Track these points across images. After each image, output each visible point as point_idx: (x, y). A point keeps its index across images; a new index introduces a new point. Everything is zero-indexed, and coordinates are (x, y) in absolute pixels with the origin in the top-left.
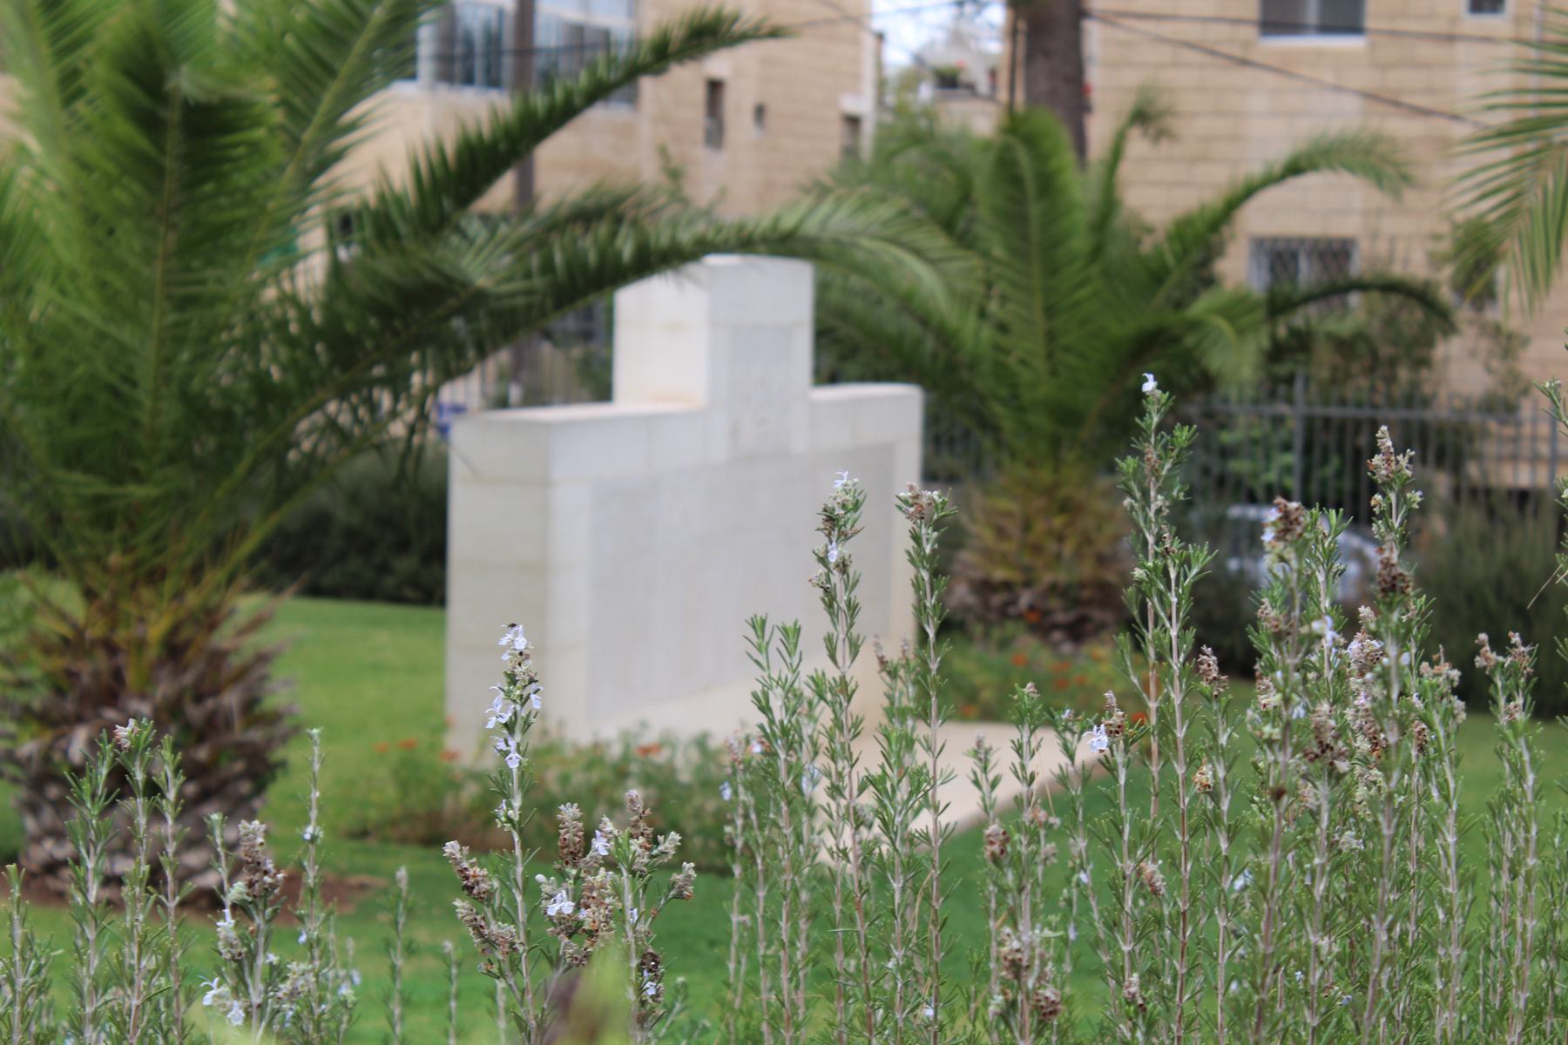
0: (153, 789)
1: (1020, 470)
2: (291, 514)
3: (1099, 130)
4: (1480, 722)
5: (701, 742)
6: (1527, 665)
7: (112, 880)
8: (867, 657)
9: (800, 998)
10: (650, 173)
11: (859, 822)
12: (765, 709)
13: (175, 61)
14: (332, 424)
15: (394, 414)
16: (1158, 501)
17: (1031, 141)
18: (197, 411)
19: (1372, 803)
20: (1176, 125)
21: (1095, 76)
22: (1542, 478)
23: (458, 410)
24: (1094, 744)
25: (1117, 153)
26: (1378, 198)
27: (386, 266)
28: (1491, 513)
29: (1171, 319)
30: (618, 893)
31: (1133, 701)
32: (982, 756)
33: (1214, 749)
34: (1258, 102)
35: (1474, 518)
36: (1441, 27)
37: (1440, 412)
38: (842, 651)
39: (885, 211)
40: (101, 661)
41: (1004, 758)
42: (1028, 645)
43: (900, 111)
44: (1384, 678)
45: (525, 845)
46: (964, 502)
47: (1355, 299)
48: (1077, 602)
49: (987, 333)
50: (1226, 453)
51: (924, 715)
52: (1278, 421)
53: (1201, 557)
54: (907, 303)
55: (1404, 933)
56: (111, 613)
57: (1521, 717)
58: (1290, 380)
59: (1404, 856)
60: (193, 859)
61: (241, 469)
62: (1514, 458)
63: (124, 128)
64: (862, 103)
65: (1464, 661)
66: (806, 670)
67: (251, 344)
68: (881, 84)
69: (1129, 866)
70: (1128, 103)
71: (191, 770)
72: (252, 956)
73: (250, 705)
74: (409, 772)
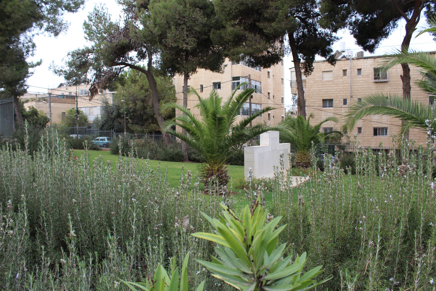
0: (216, 183)
1: (300, 151)
2: (229, 157)
3: (307, 117)
4: (346, 175)
5: (269, 178)
6: (351, 169)
7: (212, 192)
8: (285, 169)
9: (279, 203)
10: (263, 123)
11: (285, 186)
12: (275, 175)
13: (217, 114)
14: (233, 148)
15: (239, 147)
16: (313, 153)
17: (300, 119)
18: (220, 147)
19: (335, 183)
20: (315, 117)
21: (306, 112)
22: (352, 151)
23: (245, 146)
24: (308, 178)
25: (309, 119)
26: (335, 123)
27: (237, 132)
28: (347, 154)
29: (315, 136)
30: (261, 193)
31: (311, 174)
32: (297, 179)
33: (320, 178)
34: (323, 114)
35: (346, 155)
36: (340, 106)
37: (342, 144)
38: (282, 169)
39: (286, 126)
40: (211, 171)
41: (299, 179)
42: (301, 168)
43: (287, 116)
44: (336, 170)
45: (252, 188)
46: (295, 154)
47: (333, 133)
48: (306, 164)
49: (297, 137)
50: (321, 149)
51: (291, 176)
52: (326, 145)
53: (318, 159)
54: (289, 135)
55: (339, 196)
56: (212, 167)
57: (350, 174)
58: (327, 141)
59: (339, 188)
60: (220, 190)
61: (224, 153)
62: (349, 149)
63: (212, 120)
64: (284, 115)
65: (345, 169)
66: (279, 171)
67: (225, 141)
68: (285, 113)
69: (311, 190)
70: (310, 115)
71: (220, 182)
72: (226, 199)
73: (225, 175)
74: (241, 182)
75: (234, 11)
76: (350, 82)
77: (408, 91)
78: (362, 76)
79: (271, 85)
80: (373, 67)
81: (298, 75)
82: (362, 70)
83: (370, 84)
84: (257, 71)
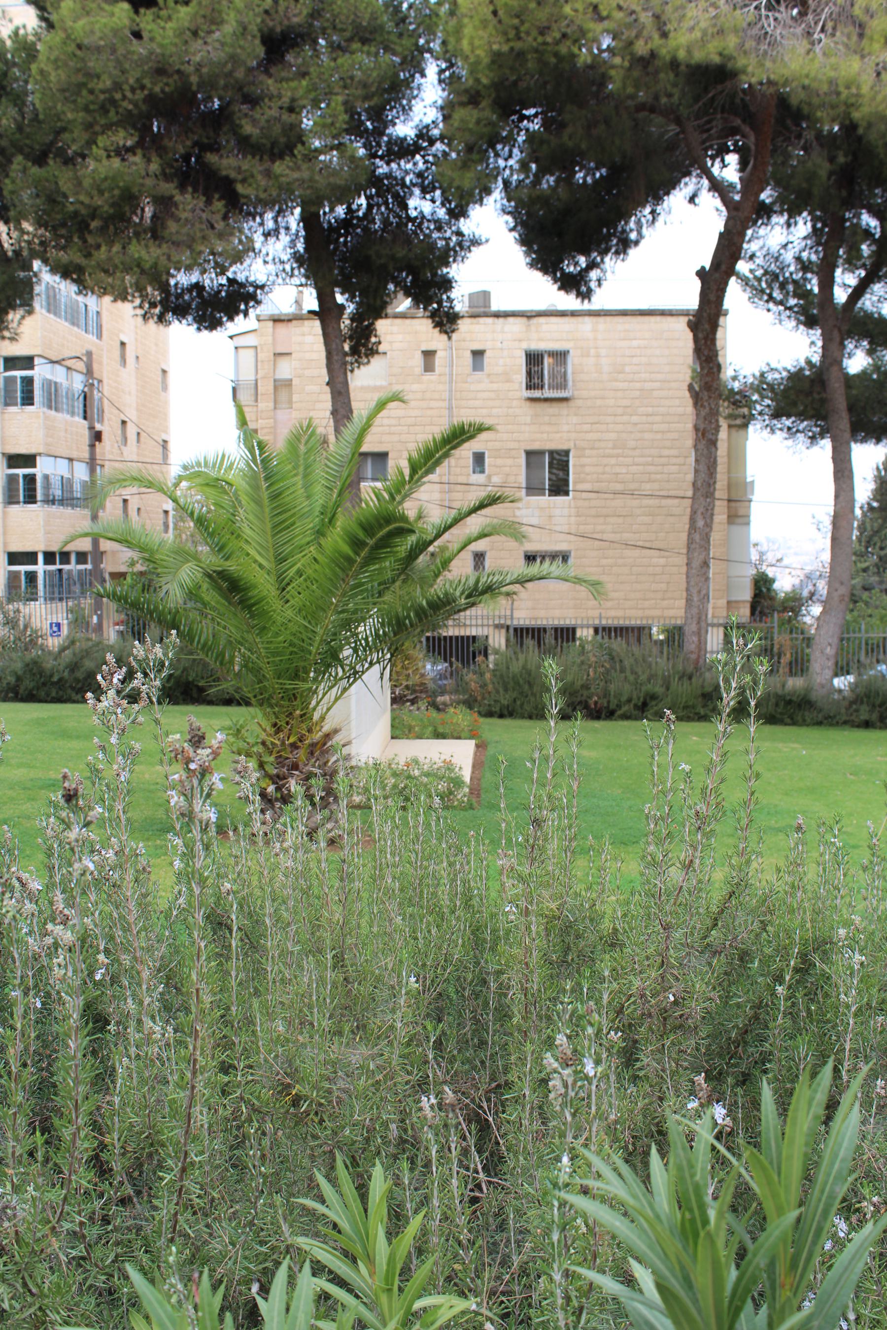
48: (414, 691)
75: (129, 95)
76: (446, 395)
77: (713, 438)
78: (489, 375)
79: (130, 393)
80: (525, 346)
81: (336, 366)
82: (487, 354)
83: (515, 403)
84: (90, 336)
